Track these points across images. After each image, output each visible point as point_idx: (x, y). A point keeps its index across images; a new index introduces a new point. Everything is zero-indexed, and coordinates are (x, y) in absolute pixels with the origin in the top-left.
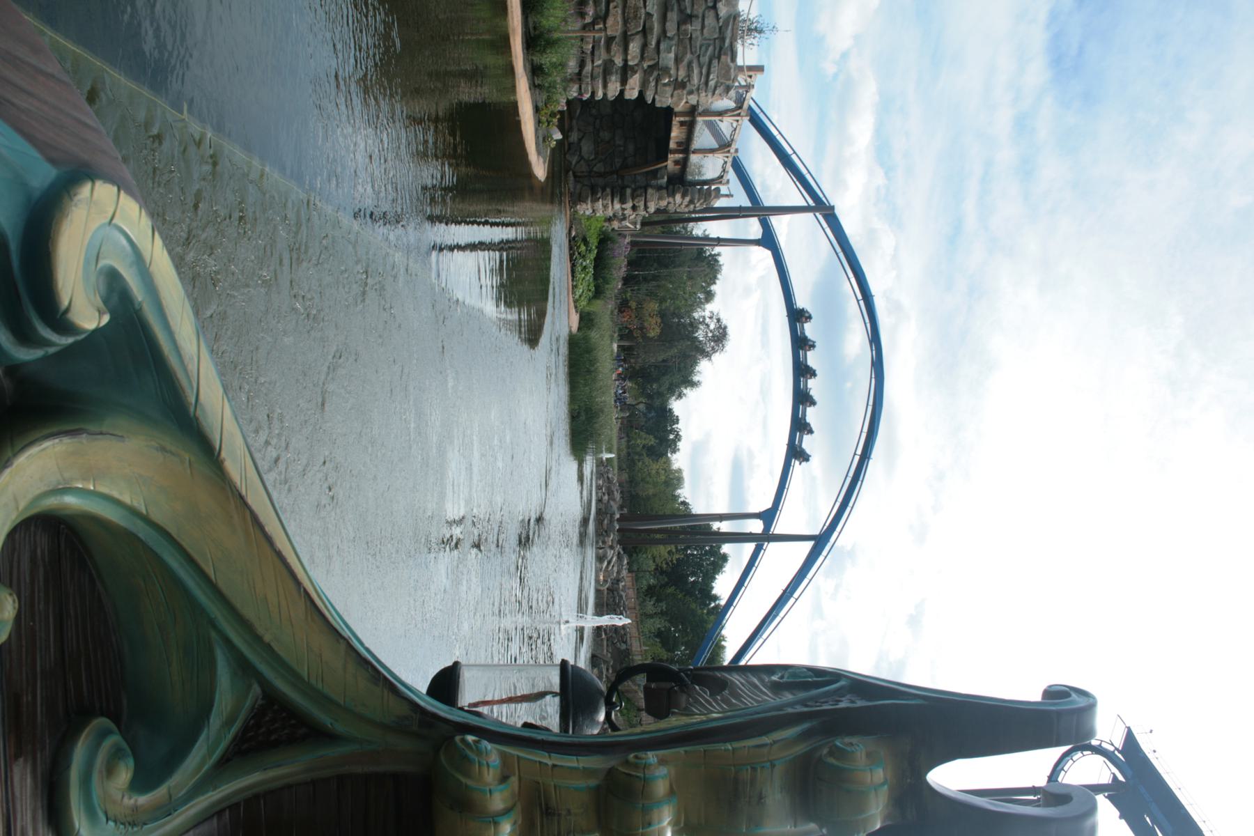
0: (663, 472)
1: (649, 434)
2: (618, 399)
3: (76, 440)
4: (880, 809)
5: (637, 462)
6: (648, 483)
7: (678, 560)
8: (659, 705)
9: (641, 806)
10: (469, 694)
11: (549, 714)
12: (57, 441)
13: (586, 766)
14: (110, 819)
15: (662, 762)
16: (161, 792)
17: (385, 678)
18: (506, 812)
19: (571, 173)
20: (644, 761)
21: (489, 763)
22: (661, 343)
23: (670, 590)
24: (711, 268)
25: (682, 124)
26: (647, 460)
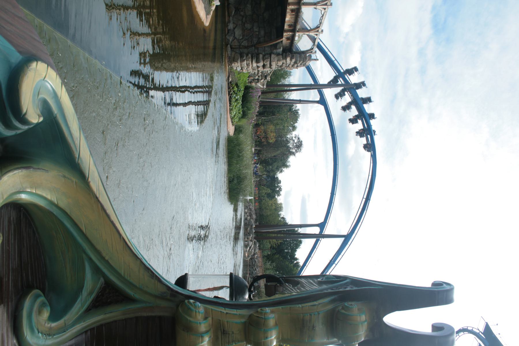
0: (274, 204)
1: (268, 188)
2: (255, 173)
3: (28, 171)
4: (363, 332)
5: (262, 200)
6: (267, 209)
7: (281, 243)
8: (270, 292)
9: (263, 330)
10: (192, 285)
11: (225, 294)
12: (20, 171)
13: (240, 313)
14: (40, 332)
15: (272, 312)
16: (61, 322)
17: (156, 276)
18: (207, 332)
19: (229, 46)
20: (264, 311)
21: (200, 311)
22: (274, 148)
23: (277, 256)
24: (295, 116)
25: (292, 11)
26: (267, 199)
